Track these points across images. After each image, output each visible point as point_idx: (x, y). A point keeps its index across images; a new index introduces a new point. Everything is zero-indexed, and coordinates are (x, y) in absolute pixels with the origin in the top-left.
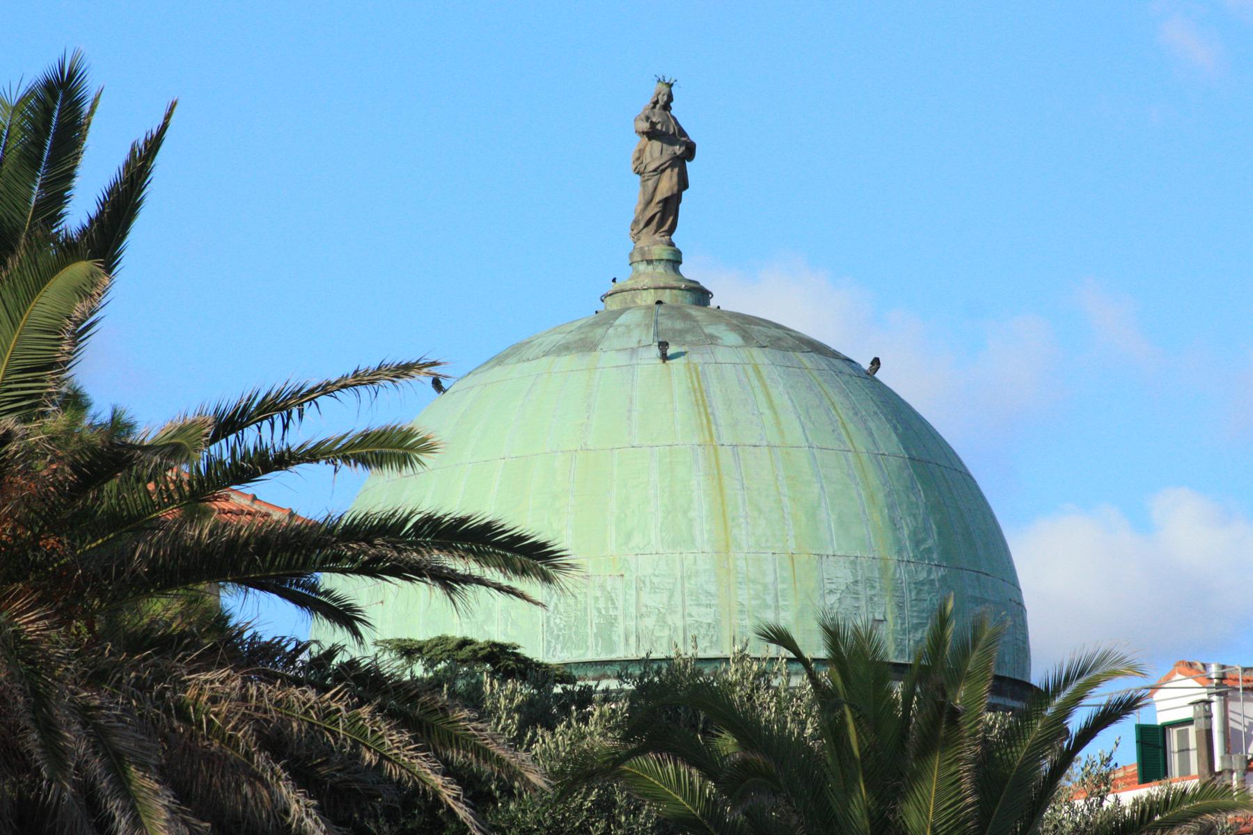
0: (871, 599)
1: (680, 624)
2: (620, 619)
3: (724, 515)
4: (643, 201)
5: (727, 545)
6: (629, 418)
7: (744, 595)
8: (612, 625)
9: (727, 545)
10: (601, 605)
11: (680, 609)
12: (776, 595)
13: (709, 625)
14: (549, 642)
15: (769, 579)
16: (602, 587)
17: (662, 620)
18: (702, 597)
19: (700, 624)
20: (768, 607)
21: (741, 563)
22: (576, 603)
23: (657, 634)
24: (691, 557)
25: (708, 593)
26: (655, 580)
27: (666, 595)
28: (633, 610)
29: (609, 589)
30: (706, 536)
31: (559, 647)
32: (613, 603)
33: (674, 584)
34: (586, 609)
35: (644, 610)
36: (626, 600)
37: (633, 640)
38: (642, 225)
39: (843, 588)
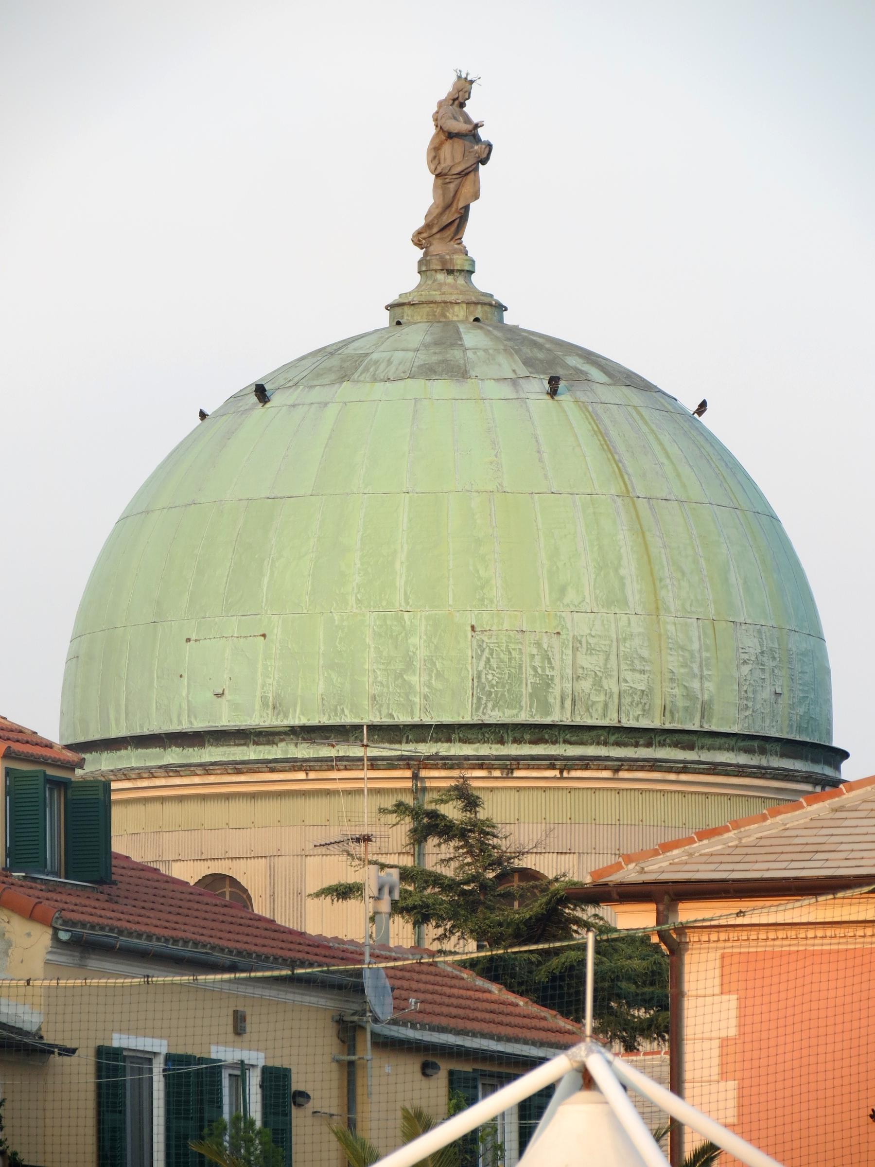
0: (773, 671)
1: (615, 690)
2: (557, 680)
3: (652, 574)
4: (441, 205)
5: (657, 609)
6: (541, 460)
7: (673, 662)
8: (548, 686)
9: (657, 609)
10: (537, 662)
11: (615, 673)
12: (701, 663)
13: (643, 691)
14: (479, 699)
15: (696, 646)
16: (538, 644)
17: (598, 684)
18: (637, 662)
19: (634, 691)
20: (695, 676)
21: (671, 628)
22: (510, 659)
23: (594, 698)
24: (625, 617)
25: (642, 658)
26: (591, 640)
27: (602, 657)
28: (569, 671)
29: (545, 646)
30: (637, 597)
31: (490, 705)
32: (550, 662)
33: (610, 646)
34: (520, 667)
35: (580, 671)
36: (562, 660)
37: (568, 703)
38: (435, 230)
39: (753, 658)
